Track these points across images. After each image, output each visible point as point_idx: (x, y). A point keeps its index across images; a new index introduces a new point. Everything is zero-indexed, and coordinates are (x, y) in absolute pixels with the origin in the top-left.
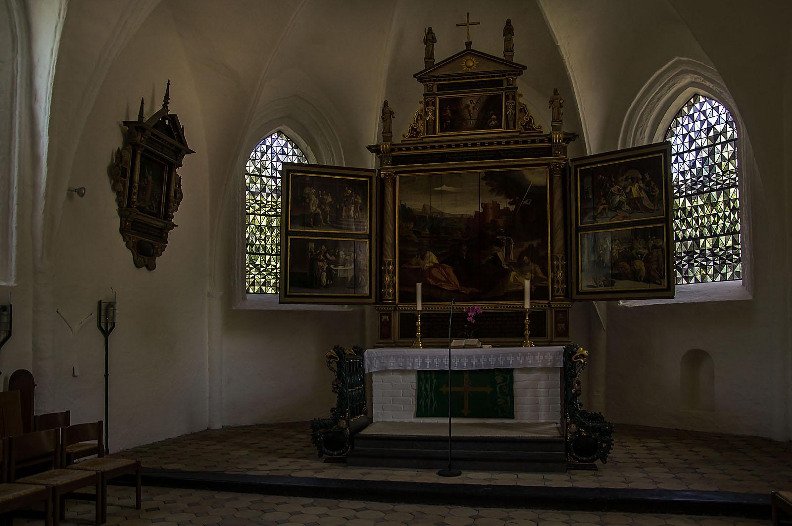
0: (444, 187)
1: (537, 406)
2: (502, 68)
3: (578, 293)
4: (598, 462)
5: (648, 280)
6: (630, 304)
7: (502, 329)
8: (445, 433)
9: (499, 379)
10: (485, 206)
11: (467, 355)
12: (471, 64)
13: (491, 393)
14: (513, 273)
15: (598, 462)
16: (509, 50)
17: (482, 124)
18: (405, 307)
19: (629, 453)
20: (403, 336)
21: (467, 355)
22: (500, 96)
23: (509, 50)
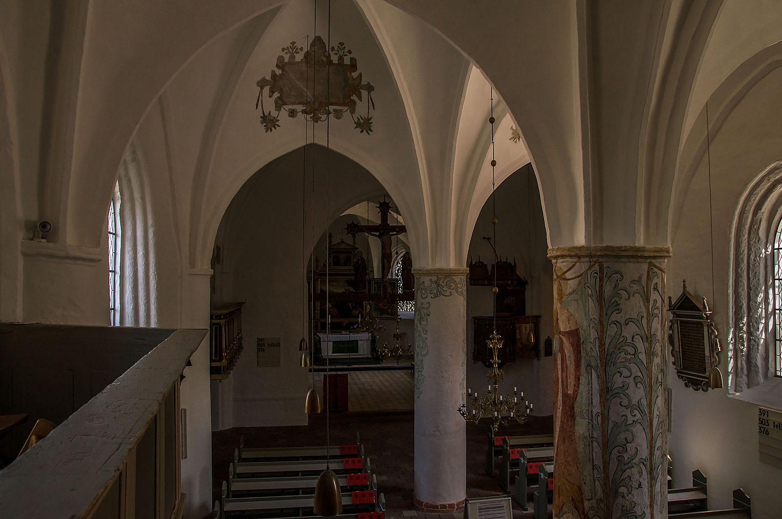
0: (334, 284)
1: (364, 350)
2: (353, 248)
3: (372, 317)
4: (381, 362)
5: (391, 315)
6: (515, 470)
7: (349, 328)
8: (348, 357)
9: (354, 342)
10: (345, 290)
11: (345, 336)
12: (343, 246)
13: (352, 346)
14: (353, 311)
15: (381, 362)
16: (354, 243)
17: (345, 264)
18: (323, 320)
19: (100, 469)
20: (321, 329)
21: (345, 336)
22: (351, 256)
23: (354, 243)
